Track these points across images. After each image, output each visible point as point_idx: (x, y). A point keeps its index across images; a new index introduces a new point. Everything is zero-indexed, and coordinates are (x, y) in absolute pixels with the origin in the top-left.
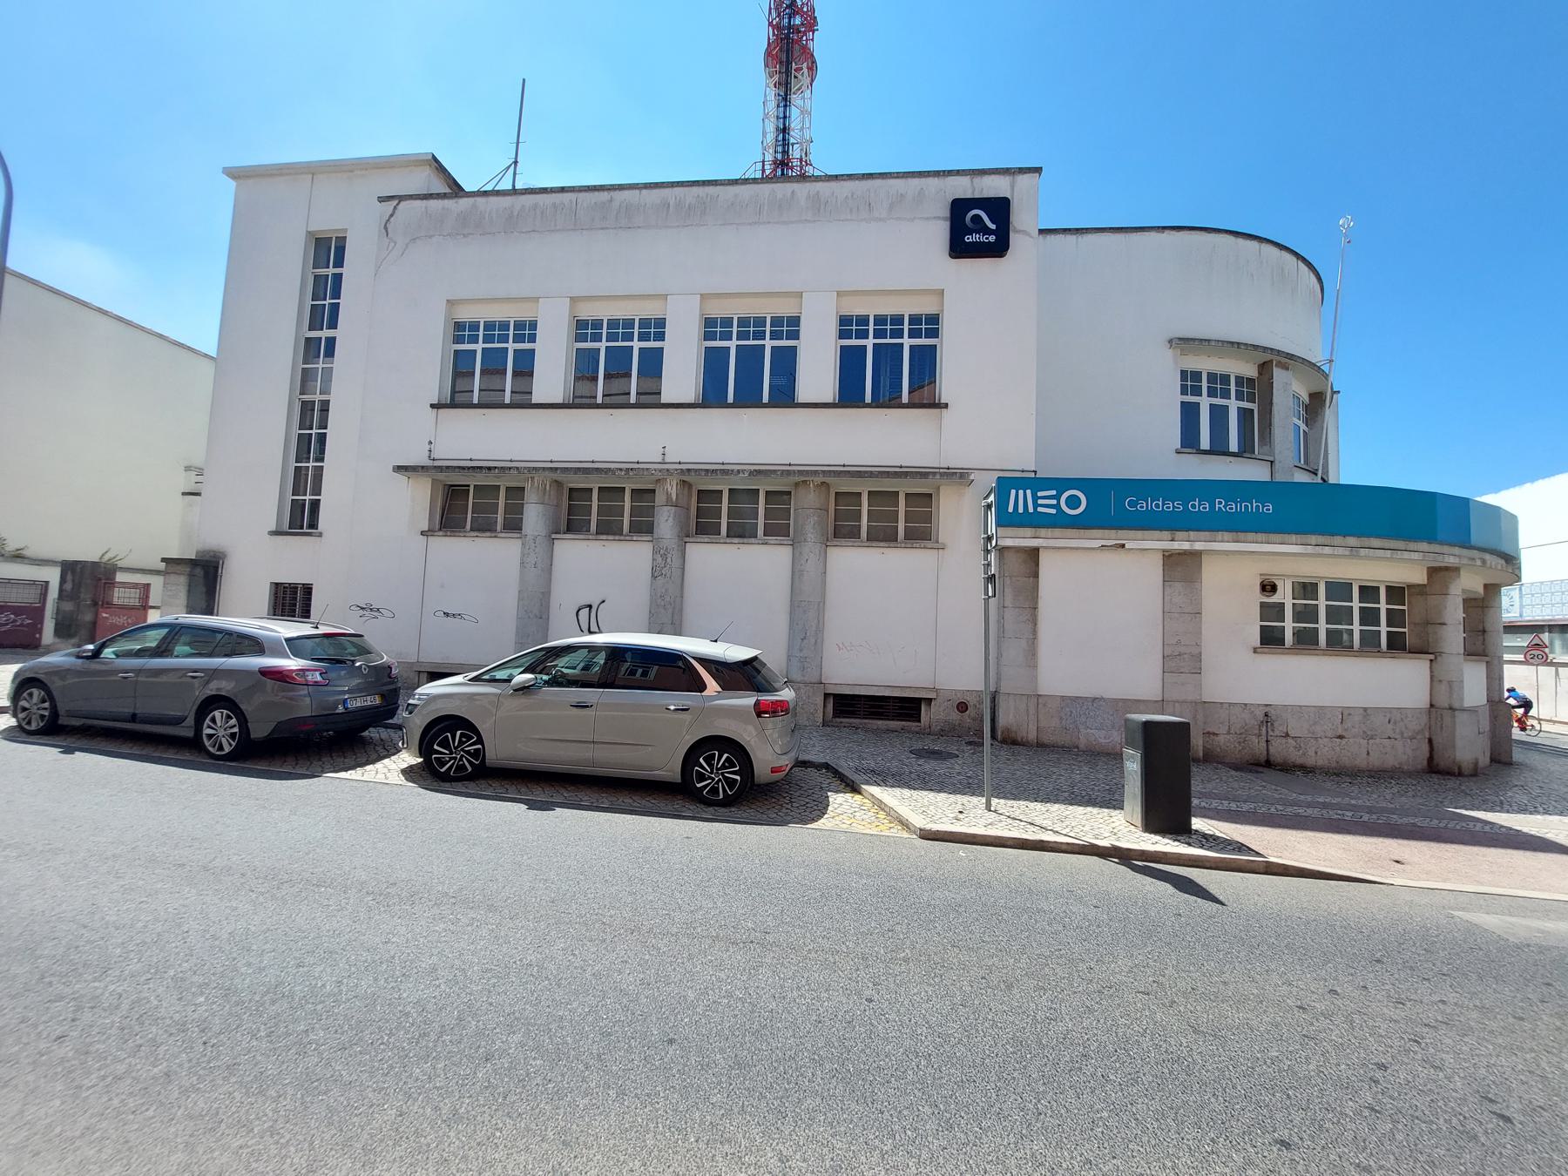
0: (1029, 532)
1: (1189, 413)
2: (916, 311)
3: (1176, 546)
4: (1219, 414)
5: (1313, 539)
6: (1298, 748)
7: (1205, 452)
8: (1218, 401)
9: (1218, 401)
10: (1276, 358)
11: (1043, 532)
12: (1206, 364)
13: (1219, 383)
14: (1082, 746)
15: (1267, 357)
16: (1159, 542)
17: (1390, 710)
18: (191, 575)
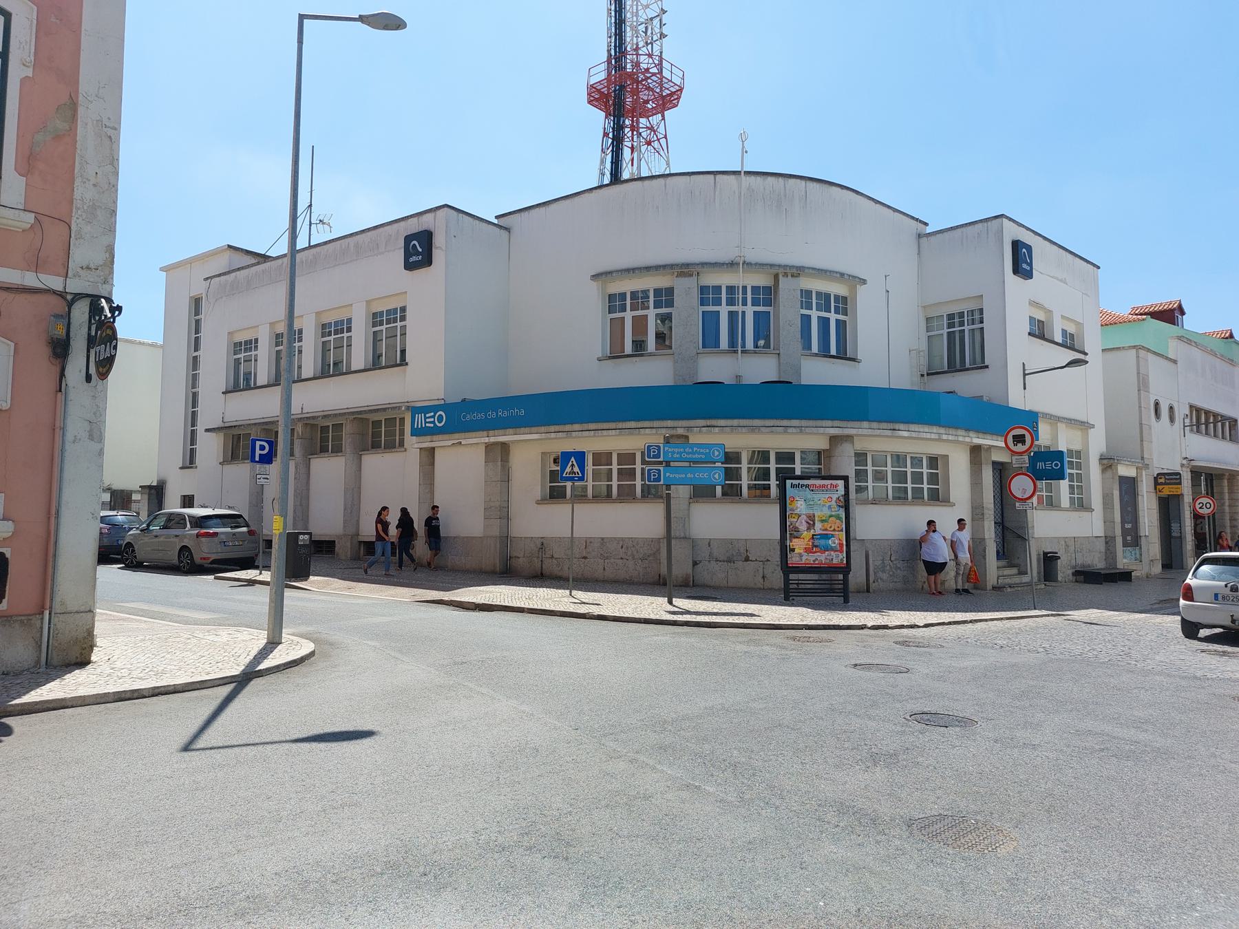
0: (429, 438)
1: (617, 328)
2: (756, 284)
3: (492, 439)
4: (639, 324)
5: (543, 429)
6: (558, 565)
7: (833, 357)
8: (841, 317)
9: (841, 317)
10: (781, 270)
11: (435, 438)
12: (617, 287)
13: (639, 299)
14: (17, 625)
15: (774, 271)
16: (483, 439)
17: (623, 539)
18: (150, 495)
